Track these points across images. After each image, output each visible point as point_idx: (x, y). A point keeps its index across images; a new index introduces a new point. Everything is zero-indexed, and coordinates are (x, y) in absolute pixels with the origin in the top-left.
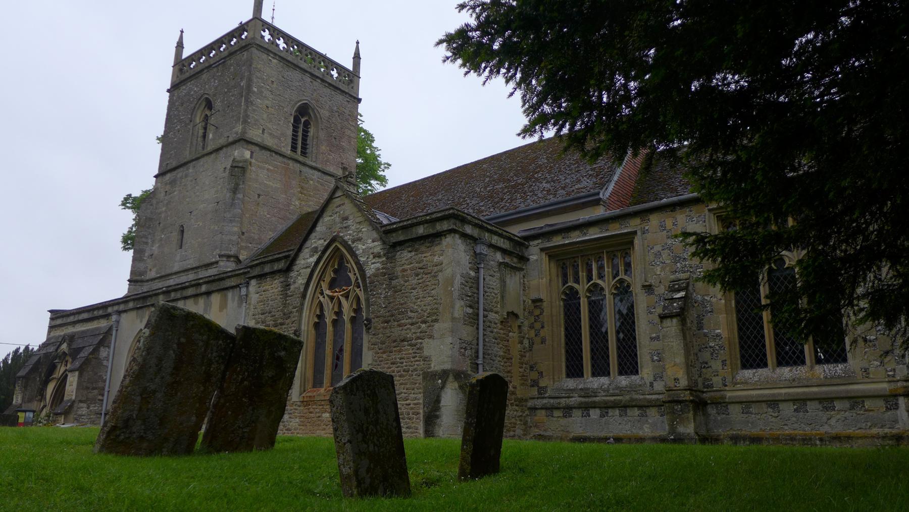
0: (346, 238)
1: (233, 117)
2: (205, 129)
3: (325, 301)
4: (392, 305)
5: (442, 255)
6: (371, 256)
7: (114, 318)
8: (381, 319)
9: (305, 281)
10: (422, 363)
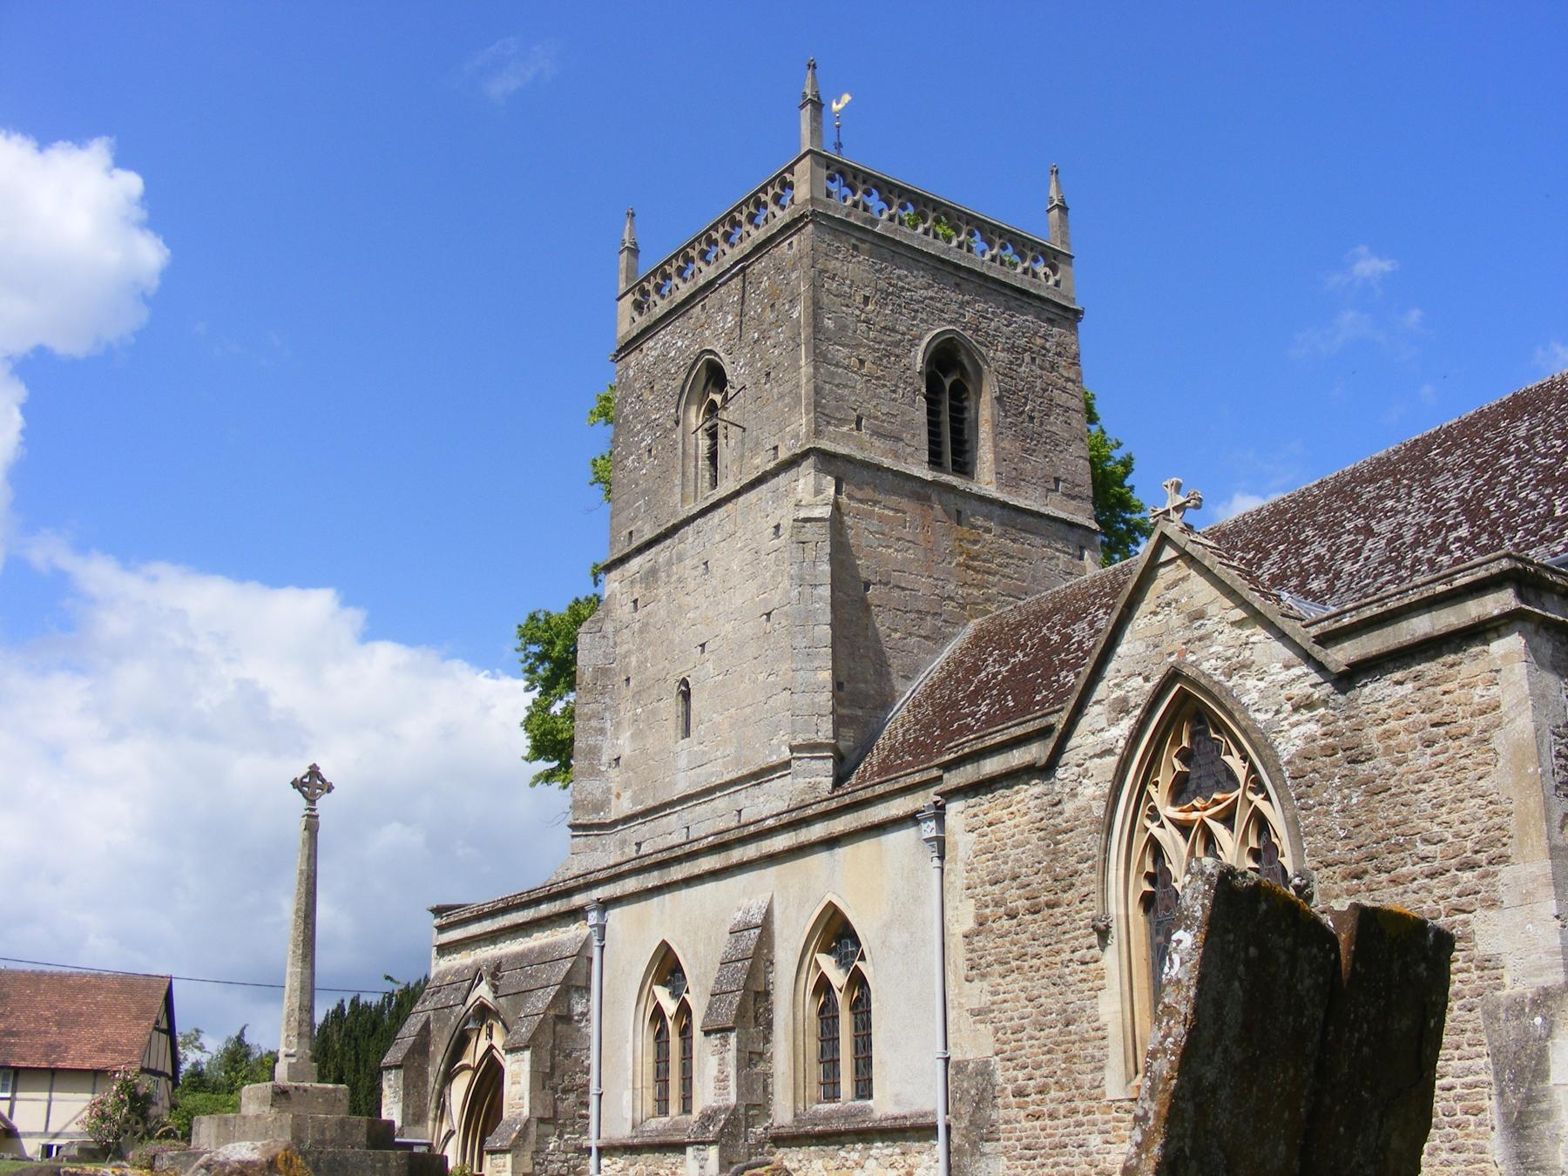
0: (1205, 666)
1: (781, 396)
2: (713, 435)
3: (1169, 837)
4: (1366, 829)
5: (1494, 682)
6: (1288, 707)
7: (593, 917)
8: (1339, 869)
9: (1107, 788)
10: (1475, 974)
